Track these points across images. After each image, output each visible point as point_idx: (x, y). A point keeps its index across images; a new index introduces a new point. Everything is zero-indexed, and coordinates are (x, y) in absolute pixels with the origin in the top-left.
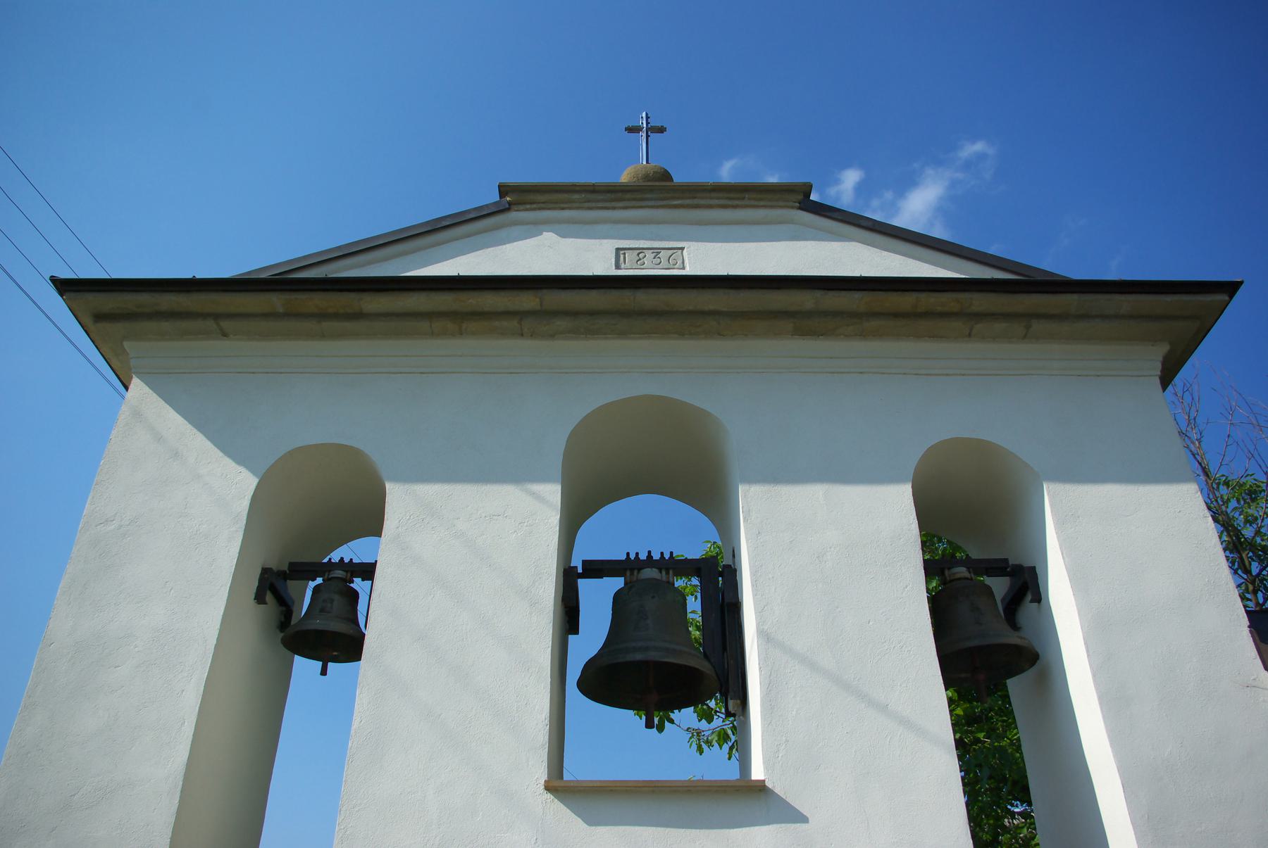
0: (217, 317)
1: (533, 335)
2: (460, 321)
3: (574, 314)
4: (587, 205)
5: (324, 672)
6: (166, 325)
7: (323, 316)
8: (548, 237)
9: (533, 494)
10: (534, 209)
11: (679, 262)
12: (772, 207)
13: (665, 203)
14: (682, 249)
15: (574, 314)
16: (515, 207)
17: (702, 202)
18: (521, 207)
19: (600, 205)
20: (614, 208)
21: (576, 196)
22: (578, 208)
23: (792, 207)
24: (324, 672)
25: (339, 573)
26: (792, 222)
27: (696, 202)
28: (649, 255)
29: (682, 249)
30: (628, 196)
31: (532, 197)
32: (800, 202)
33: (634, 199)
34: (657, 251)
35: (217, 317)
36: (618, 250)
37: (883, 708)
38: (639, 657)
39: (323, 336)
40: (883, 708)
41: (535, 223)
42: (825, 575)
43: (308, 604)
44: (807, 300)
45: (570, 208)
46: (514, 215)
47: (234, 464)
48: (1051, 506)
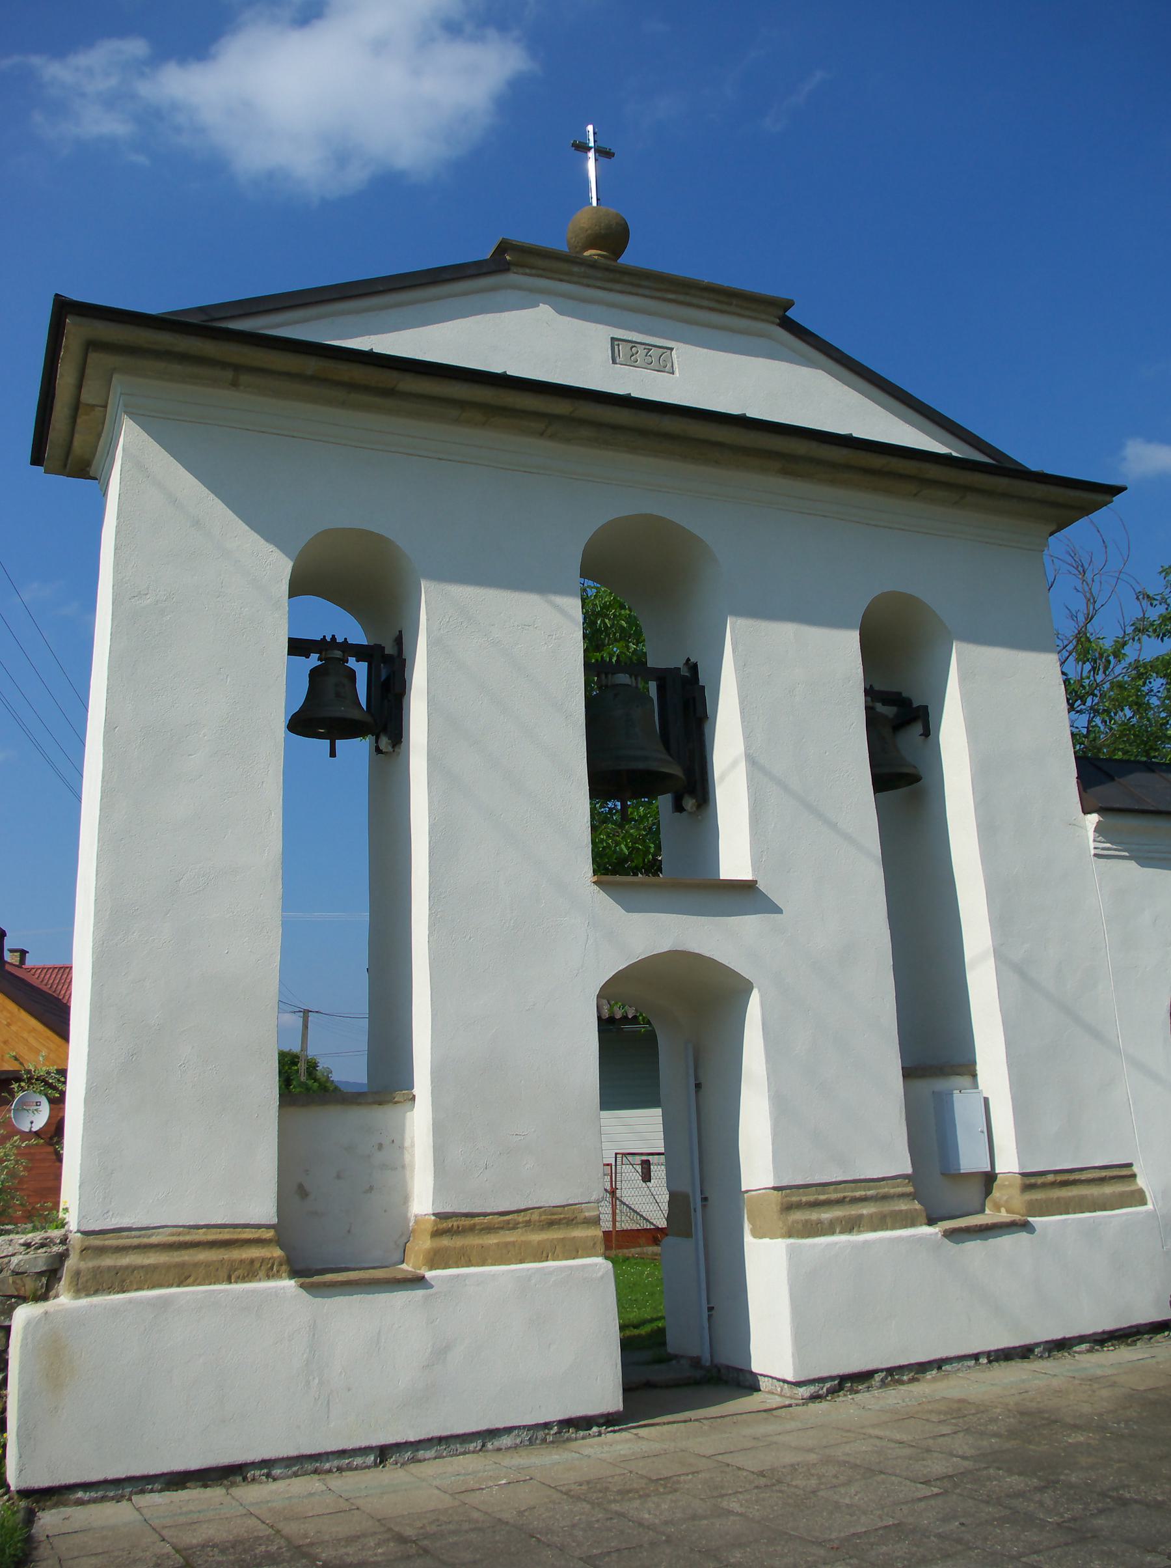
0: (237, 368)
1: (552, 437)
2: (491, 413)
3: (599, 425)
4: (585, 281)
5: (333, 754)
6: (177, 368)
7: (352, 386)
8: (544, 311)
9: (557, 607)
10: (531, 275)
11: (669, 365)
12: (755, 319)
13: (659, 294)
14: (672, 349)
15: (599, 425)
16: (514, 269)
17: (695, 301)
18: (521, 270)
19: (599, 284)
20: (611, 290)
21: (576, 269)
22: (575, 283)
23: (773, 323)
24: (333, 754)
25: (338, 654)
26: (760, 335)
27: (688, 299)
28: (641, 351)
29: (672, 349)
30: (626, 279)
31: (540, 263)
32: (774, 319)
33: (632, 284)
34: (649, 347)
35: (237, 368)
36: (613, 339)
37: (833, 826)
38: (641, 766)
39: (343, 404)
40: (833, 826)
41: (531, 290)
42: (776, 704)
43: (351, 698)
44: (801, 447)
45: (569, 282)
46: (512, 277)
47: (262, 541)
48: (962, 680)
